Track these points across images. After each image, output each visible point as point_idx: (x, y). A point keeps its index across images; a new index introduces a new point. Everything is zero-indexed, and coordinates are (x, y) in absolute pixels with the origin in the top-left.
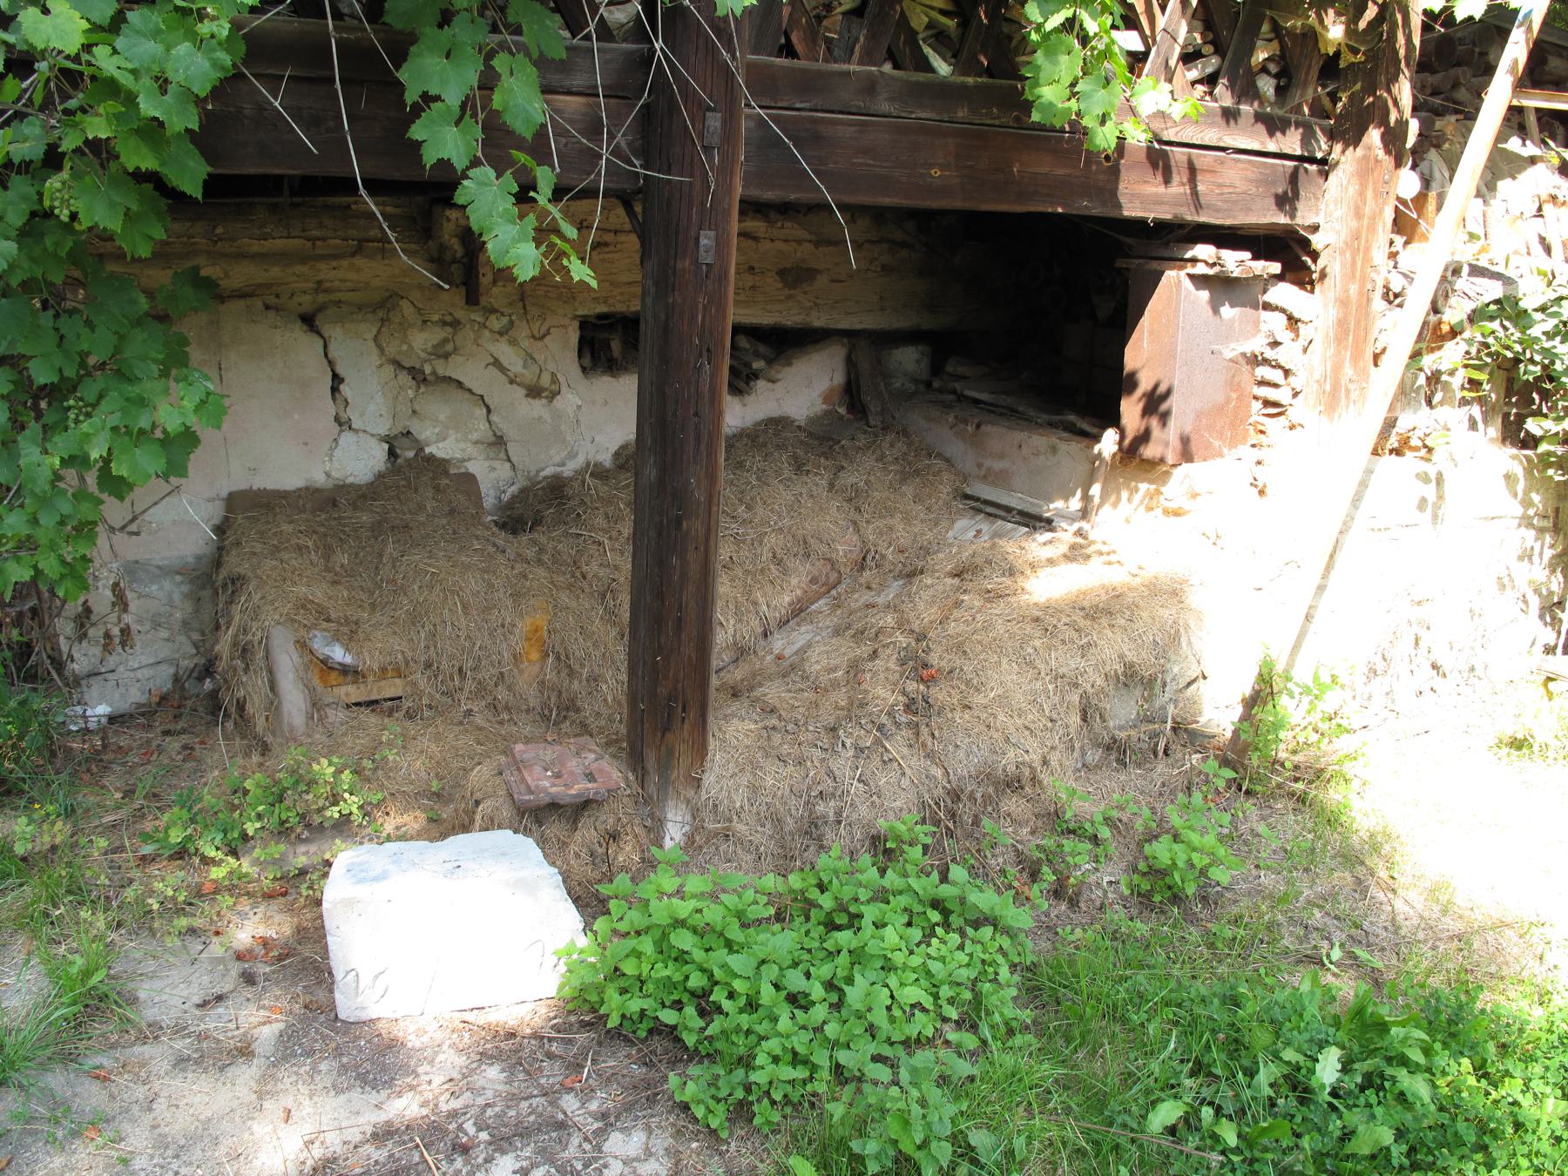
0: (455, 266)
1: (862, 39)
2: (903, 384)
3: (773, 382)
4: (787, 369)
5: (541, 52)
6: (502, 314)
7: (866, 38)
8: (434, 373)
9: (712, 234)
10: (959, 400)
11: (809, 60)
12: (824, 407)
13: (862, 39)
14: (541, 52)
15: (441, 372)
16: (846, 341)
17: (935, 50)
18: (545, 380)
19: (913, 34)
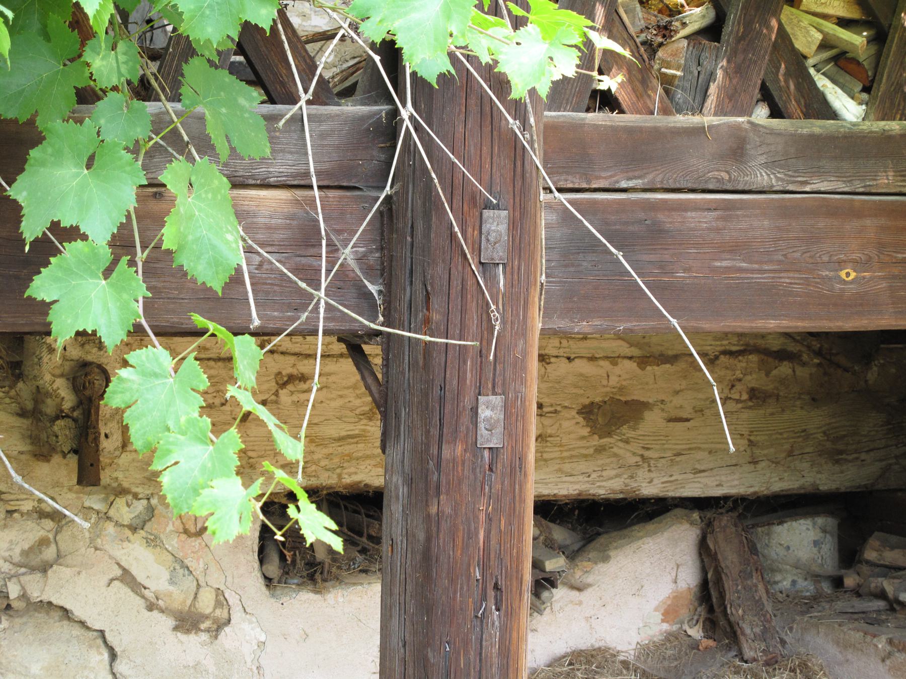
0: (60, 423)
1: (720, 74)
2: (794, 582)
3: (579, 589)
4: (601, 567)
5: (233, 149)
6: (136, 496)
7: (726, 71)
8: (24, 596)
9: (497, 400)
10: (892, 609)
11: (638, 112)
12: (665, 627)
13: (720, 74)
14: (233, 149)
15: (35, 594)
16: (696, 515)
17: (834, 81)
18: (206, 602)
19: (799, 59)
